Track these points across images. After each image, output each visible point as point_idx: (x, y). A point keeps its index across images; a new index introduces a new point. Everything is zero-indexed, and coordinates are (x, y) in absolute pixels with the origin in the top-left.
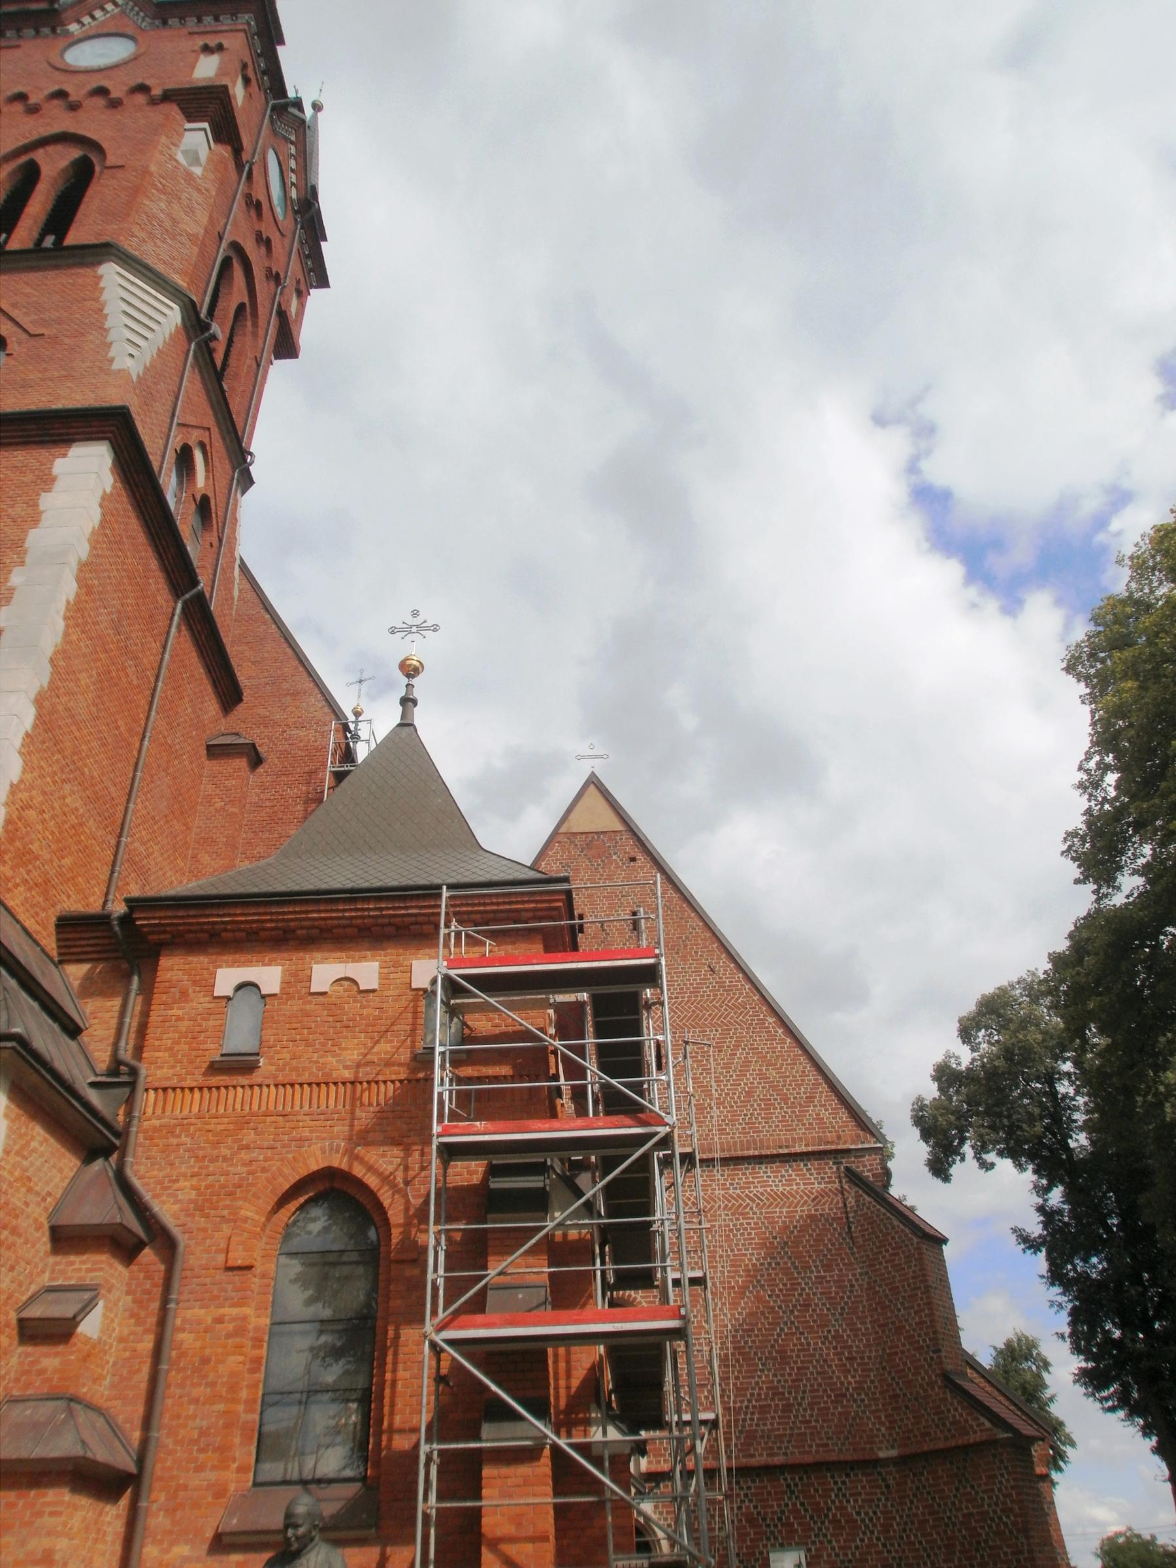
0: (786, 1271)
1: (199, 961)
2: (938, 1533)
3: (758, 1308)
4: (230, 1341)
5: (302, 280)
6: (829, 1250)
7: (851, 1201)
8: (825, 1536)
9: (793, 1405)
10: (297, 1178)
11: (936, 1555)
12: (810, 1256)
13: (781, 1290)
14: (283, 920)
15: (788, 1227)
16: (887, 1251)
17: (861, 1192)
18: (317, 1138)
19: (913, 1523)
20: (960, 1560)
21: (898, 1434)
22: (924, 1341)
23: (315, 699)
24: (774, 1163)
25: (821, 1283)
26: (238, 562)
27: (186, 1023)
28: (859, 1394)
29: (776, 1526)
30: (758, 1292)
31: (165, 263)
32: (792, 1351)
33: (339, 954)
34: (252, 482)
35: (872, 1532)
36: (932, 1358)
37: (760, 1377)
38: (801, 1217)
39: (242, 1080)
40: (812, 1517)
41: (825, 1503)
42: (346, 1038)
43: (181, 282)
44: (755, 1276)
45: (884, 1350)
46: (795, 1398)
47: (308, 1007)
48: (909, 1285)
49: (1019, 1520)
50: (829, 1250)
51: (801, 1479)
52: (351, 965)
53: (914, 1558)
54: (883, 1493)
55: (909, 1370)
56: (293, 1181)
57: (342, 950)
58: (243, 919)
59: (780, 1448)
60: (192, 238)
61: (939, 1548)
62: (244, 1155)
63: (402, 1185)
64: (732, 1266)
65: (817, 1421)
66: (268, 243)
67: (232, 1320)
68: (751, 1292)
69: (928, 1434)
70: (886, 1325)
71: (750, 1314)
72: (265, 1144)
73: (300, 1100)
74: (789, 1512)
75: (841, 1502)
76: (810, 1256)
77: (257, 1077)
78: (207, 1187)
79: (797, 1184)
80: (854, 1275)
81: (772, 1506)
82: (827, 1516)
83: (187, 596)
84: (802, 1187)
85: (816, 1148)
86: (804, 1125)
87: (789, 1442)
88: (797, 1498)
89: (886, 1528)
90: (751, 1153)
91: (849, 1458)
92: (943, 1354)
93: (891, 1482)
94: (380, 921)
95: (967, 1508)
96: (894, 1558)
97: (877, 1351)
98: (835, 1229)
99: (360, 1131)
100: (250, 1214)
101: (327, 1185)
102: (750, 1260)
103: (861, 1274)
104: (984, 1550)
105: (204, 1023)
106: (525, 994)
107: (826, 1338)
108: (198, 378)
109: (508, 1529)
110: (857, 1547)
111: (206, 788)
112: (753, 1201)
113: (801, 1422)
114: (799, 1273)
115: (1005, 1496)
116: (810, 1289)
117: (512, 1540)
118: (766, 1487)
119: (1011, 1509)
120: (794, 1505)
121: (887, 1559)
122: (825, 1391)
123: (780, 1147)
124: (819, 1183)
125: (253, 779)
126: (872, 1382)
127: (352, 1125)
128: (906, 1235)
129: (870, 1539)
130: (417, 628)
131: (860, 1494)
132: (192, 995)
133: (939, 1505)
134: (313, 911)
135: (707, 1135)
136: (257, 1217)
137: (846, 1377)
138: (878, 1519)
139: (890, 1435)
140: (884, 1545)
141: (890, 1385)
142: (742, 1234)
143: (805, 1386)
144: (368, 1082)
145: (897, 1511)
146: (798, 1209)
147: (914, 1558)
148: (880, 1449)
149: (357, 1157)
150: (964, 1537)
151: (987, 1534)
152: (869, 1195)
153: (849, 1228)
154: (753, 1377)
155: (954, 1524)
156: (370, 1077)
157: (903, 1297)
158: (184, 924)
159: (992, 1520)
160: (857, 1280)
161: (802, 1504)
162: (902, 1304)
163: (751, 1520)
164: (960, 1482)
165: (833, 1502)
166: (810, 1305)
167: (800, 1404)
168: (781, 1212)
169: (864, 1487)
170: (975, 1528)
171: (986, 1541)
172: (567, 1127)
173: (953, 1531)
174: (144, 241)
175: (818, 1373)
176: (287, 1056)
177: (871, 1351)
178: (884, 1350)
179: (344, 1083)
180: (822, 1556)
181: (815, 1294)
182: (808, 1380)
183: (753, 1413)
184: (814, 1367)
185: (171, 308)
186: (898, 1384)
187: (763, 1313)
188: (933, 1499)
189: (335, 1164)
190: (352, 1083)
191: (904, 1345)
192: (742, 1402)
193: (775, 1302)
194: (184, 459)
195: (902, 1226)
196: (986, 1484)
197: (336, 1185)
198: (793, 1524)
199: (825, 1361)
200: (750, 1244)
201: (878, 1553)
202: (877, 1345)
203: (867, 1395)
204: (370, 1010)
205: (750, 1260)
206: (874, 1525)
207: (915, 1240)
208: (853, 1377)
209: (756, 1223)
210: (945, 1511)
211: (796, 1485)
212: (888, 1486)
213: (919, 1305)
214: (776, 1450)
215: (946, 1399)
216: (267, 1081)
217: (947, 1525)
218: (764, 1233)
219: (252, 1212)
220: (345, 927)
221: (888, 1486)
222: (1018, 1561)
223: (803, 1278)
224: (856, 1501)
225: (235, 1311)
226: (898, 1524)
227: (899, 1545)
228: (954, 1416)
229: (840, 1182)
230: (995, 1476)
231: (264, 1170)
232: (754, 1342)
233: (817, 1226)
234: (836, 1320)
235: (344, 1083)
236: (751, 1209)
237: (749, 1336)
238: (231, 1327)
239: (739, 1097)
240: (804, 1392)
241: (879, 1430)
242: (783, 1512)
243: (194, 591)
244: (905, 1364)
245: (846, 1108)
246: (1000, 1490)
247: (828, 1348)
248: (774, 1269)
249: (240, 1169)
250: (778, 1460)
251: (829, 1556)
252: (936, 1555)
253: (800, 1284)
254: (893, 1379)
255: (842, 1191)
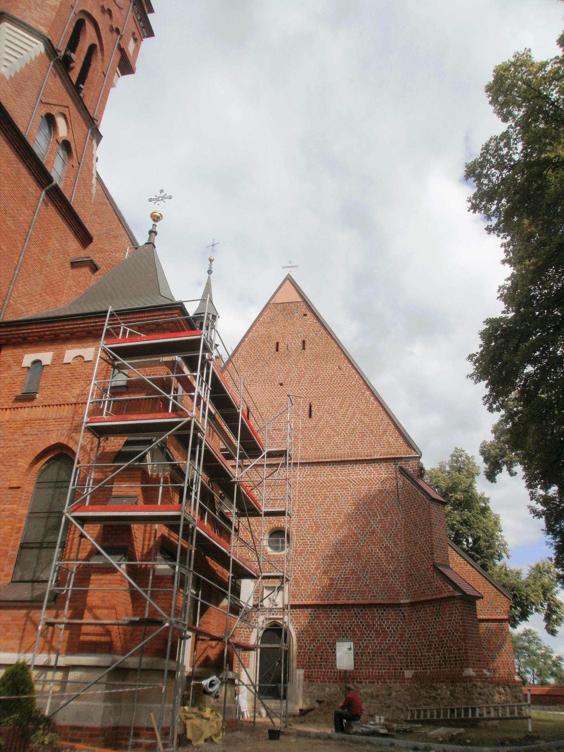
0: (365, 517)
1: (18, 351)
2: (425, 639)
3: (349, 533)
4: (6, 519)
5: (137, 32)
6: (387, 507)
7: (401, 483)
8: (371, 637)
9: (361, 578)
10: (45, 448)
11: (423, 649)
12: (377, 510)
13: (361, 525)
14: (54, 330)
15: (368, 495)
16: (414, 507)
17: (405, 479)
18: (56, 430)
19: (414, 634)
20: (434, 652)
21: (411, 592)
22: (427, 549)
23: (125, 238)
24: (363, 464)
25: (381, 522)
26: (95, 176)
27: (8, 380)
28: (394, 574)
29: (348, 631)
30: (350, 526)
31: (36, 21)
32: (363, 553)
33: (78, 345)
34: (101, 136)
35: (394, 637)
36: (429, 557)
37: (346, 565)
38: (374, 490)
39: (28, 404)
40: (365, 628)
41: (373, 622)
42: (75, 383)
43: (44, 30)
44: (349, 519)
45: (408, 553)
46: (363, 575)
47: (62, 370)
48: (423, 523)
49: (462, 635)
50: (387, 507)
51: (362, 611)
52: (83, 350)
53: (413, 650)
54: (401, 619)
55: (419, 562)
56: (42, 449)
57: (80, 343)
58: (36, 330)
59: (353, 597)
60: (53, 8)
61: (425, 646)
62: (24, 438)
63: (89, 450)
64: (337, 514)
65: (372, 585)
66: (109, 12)
67: (8, 511)
68: (346, 526)
69: (424, 593)
70: (411, 542)
71: (345, 536)
72: (34, 433)
73: (52, 413)
74: (355, 625)
75: (380, 622)
76: (377, 510)
77: (34, 403)
78: (7, 453)
79: (374, 474)
80: (398, 519)
81: (347, 622)
82: (373, 628)
83: (47, 188)
84: (376, 476)
85: (385, 457)
86: (380, 445)
87: (357, 594)
88: (359, 619)
89: (402, 636)
90: (352, 459)
91: (386, 602)
92: (435, 555)
93: (406, 614)
94: (96, 328)
95: (439, 628)
96: (404, 650)
97: (405, 554)
98: (391, 497)
99: (75, 426)
100: (21, 464)
101: (59, 452)
102: (347, 511)
103: (402, 518)
104: (445, 648)
105: (16, 379)
106: (143, 358)
107: (381, 548)
108: (59, 80)
109: (98, 603)
110: (386, 644)
111: (70, 282)
112: (351, 482)
113: (364, 585)
114: (371, 517)
115: (456, 623)
116: (376, 525)
117: (99, 607)
118: (344, 614)
119: (458, 630)
120: (357, 622)
121: (401, 650)
122: (378, 572)
123: (367, 456)
124: (385, 474)
125: (93, 277)
126: (401, 568)
127: (72, 424)
128: (424, 499)
129: (393, 640)
130: (163, 197)
131: (390, 619)
132: (13, 367)
133: (427, 626)
134: (66, 325)
135: (331, 450)
136: (25, 465)
137: (389, 566)
138: (398, 631)
139: (408, 593)
140: (400, 643)
141: (409, 570)
142: (344, 498)
143: (368, 569)
144: (82, 403)
145: (408, 628)
146: (374, 487)
147: (413, 650)
148: (402, 599)
149: (72, 438)
150: (436, 641)
151: (447, 641)
152: (409, 480)
153: (398, 496)
154: (343, 565)
155: (432, 635)
156: (82, 401)
157: (420, 529)
158: (11, 334)
159: (450, 634)
160: (399, 521)
161: (361, 622)
162: (419, 532)
163: (336, 628)
164: (437, 615)
165: (376, 622)
166: (375, 533)
167: (365, 577)
168: (365, 488)
169: (392, 616)
170: (442, 638)
171: (446, 644)
172: (144, 418)
173: (431, 639)
174: (25, 10)
175: (375, 564)
176: (49, 392)
177: (402, 554)
178: (408, 553)
179: (71, 404)
180: (369, 647)
181: (377, 527)
182: (370, 566)
183: (341, 581)
184: (374, 561)
185: (37, 44)
186: (413, 569)
187: (351, 536)
188: (424, 623)
189: (61, 442)
190: (75, 404)
191: (417, 551)
192: (336, 575)
193: (357, 531)
194: (50, 120)
195: (422, 495)
196: (448, 617)
197: (63, 451)
198: (356, 631)
199: (379, 558)
200: (348, 503)
201: (396, 647)
202: (406, 551)
203: (398, 574)
204: (88, 370)
205: (347, 511)
206: (396, 634)
207: (428, 501)
208: (392, 566)
209: (351, 493)
210: (429, 629)
211: (359, 613)
212: (404, 616)
213: (426, 533)
214: (351, 598)
215: (434, 576)
216: (39, 404)
217: (429, 635)
218: (355, 498)
219: (24, 463)
220: (81, 332)
221: (404, 616)
222: (460, 653)
223: (373, 520)
224: (388, 622)
225: (10, 506)
226: (408, 634)
227: (407, 644)
228: (437, 585)
229: (396, 474)
230: (453, 614)
231: (32, 444)
232: (345, 549)
233: (382, 495)
234: (387, 540)
235: (71, 404)
236: (350, 486)
237: (343, 546)
238: (8, 513)
239: (349, 431)
240: (367, 572)
241: (403, 590)
242: (351, 625)
243: (51, 185)
244: (417, 560)
245: (403, 437)
246: (454, 620)
247: (381, 553)
248: (358, 515)
249: (22, 444)
250: (351, 602)
251: (372, 646)
252: (423, 649)
253: (371, 522)
254: (411, 567)
255: (396, 478)
